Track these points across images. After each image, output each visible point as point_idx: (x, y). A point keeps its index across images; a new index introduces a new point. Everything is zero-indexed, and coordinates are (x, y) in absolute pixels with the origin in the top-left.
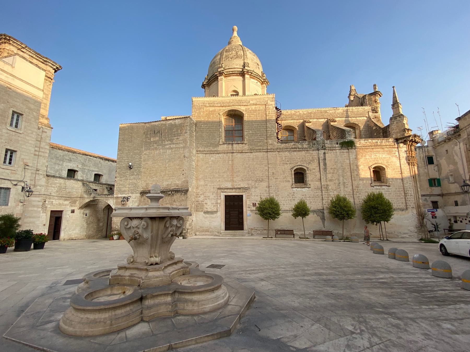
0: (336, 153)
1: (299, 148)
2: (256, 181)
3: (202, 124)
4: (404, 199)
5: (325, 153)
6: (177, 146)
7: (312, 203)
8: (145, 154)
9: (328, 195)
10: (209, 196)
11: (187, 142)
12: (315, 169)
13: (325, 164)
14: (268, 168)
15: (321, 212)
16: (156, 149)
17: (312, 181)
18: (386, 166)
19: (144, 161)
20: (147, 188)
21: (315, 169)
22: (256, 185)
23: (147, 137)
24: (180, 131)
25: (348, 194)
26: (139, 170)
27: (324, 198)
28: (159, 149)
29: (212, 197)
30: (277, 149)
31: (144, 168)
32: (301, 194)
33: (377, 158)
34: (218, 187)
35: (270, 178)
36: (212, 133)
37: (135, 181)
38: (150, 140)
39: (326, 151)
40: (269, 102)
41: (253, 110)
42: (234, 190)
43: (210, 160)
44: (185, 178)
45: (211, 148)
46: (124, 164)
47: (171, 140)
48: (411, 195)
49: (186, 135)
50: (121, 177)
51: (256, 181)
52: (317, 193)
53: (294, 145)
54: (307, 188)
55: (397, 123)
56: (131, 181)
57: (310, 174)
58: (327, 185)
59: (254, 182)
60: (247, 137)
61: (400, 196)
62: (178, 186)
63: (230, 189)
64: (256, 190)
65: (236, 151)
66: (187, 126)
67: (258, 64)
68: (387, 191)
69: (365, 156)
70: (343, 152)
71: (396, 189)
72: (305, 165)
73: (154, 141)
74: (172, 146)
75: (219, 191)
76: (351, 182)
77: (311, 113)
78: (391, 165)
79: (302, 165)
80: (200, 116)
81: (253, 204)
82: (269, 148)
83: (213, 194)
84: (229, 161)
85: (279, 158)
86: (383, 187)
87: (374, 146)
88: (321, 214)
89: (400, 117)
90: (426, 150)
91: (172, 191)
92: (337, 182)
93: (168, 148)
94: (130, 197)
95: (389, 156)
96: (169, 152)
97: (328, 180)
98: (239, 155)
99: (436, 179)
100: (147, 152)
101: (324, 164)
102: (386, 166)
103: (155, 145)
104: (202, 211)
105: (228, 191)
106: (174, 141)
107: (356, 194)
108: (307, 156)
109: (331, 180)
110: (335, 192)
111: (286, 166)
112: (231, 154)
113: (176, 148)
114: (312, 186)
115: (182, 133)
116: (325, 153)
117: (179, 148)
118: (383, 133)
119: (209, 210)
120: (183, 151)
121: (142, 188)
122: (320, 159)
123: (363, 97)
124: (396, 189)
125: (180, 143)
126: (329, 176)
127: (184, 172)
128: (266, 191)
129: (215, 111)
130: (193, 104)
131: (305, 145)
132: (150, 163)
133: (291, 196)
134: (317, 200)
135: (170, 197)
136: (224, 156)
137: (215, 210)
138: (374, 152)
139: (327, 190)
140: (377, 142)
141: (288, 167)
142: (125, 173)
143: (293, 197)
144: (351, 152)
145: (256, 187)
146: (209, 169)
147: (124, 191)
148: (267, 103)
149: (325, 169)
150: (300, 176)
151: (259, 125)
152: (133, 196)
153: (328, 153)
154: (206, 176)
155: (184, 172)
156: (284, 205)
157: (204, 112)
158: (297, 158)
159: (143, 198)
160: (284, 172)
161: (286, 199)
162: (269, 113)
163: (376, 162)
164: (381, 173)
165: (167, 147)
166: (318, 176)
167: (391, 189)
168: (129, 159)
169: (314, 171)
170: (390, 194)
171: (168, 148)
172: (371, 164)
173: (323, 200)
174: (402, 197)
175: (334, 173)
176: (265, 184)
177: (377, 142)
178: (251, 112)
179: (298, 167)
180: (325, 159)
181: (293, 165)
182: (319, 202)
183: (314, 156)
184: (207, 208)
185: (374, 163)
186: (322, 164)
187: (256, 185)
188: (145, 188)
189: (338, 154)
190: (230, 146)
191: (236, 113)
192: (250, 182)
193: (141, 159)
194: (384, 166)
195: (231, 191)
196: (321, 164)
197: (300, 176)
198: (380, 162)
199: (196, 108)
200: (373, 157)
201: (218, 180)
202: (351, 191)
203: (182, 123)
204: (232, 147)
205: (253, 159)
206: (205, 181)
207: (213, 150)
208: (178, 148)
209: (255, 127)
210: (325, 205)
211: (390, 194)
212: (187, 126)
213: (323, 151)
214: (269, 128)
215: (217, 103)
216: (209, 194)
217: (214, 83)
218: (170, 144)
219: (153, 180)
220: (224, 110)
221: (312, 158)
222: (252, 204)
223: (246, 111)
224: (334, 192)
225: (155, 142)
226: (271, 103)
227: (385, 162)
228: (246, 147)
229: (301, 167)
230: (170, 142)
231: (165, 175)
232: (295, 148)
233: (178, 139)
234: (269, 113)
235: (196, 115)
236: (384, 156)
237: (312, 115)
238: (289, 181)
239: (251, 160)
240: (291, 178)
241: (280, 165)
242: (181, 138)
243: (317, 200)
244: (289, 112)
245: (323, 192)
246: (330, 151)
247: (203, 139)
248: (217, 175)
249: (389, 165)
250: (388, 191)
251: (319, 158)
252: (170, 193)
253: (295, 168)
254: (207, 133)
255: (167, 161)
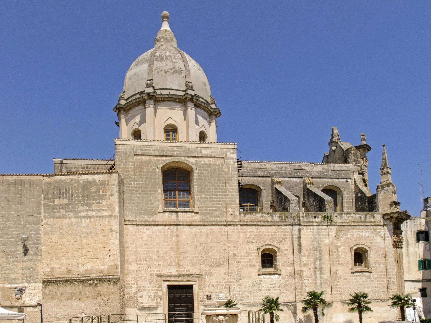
0: (313, 229)
1: (268, 221)
2: (211, 265)
3: (131, 181)
4: (385, 288)
5: (299, 230)
6: (99, 214)
7: (283, 294)
8: (46, 224)
9: (302, 283)
10: (144, 287)
11: (115, 210)
12: (287, 250)
13: (300, 245)
14: (228, 247)
15: (292, 305)
16: (64, 217)
17: (283, 265)
18: (369, 247)
19: (45, 233)
20: (54, 275)
21: (287, 250)
22: (211, 271)
23: (48, 198)
24: (103, 192)
25: (326, 283)
26: (37, 248)
27: (297, 287)
28: (70, 218)
29: (148, 287)
30: (240, 221)
31: (45, 245)
32: (272, 285)
33: (360, 238)
34: (157, 273)
35: (230, 262)
36: (146, 194)
37: (32, 264)
38: (54, 202)
39: (302, 227)
40: (228, 154)
41: (206, 164)
42: (180, 279)
43: (144, 235)
44: (113, 261)
45: (146, 218)
46: (11, 238)
47: (89, 205)
48: (393, 283)
49: (111, 198)
50: (8, 258)
51: (211, 265)
52: (288, 280)
53: (262, 216)
54: (277, 276)
55: (384, 193)
56: (24, 264)
57: (281, 256)
58: (301, 271)
59: (208, 266)
60: (198, 203)
61: (382, 284)
62: (102, 272)
63: (175, 276)
64: (212, 277)
65: (183, 222)
66: (113, 185)
67: (205, 85)
68: (368, 278)
69: (346, 235)
70: (321, 229)
71: (378, 275)
72: (275, 244)
73: (60, 205)
74: (90, 214)
75: (160, 279)
76: (329, 266)
77: (282, 168)
78: (375, 246)
79: (271, 245)
80: (128, 168)
81: (207, 296)
82: (229, 220)
83: (150, 283)
84: (173, 236)
85: (242, 235)
86: (365, 273)
87: (357, 222)
88: (292, 308)
89: (388, 186)
90: (418, 223)
91: (94, 280)
92: (312, 266)
93: (84, 217)
94: (26, 287)
95: (373, 235)
96: (86, 222)
97: (302, 265)
98: (187, 228)
99: (427, 259)
100: (50, 221)
101: (298, 244)
102: (369, 247)
103: (63, 212)
104: (135, 307)
105: (173, 279)
106: (93, 207)
107: (334, 282)
108: (278, 232)
109: (305, 265)
110: (310, 279)
111: (251, 245)
112: (175, 227)
113: (97, 217)
114: (283, 273)
115: (106, 195)
116: (299, 230)
117: (103, 217)
118: (369, 204)
119: (146, 305)
120: (109, 221)
121: (45, 274)
122: (294, 237)
123: (347, 150)
124: (378, 275)
125: (103, 210)
126: (304, 259)
127: (111, 253)
128: (224, 279)
129: (149, 161)
130: (116, 149)
131: (276, 218)
132: (55, 237)
133: (257, 285)
134: (289, 290)
135: (91, 288)
136: (164, 229)
137: (154, 305)
138: (357, 229)
139: (301, 277)
140: (360, 217)
141: (253, 247)
142: (15, 251)
143: (259, 287)
144: (331, 229)
145: (211, 274)
146: (144, 247)
147: (15, 279)
148: (226, 155)
149: (300, 251)
150: (268, 259)
151: (214, 186)
152: (31, 286)
153: (303, 229)
154: (140, 258)
155: (111, 253)
156: (248, 296)
157: (133, 162)
158: (265, 235)
159: (47, 289)
160: (248, 253)
161: (251, 289)
162: (229, 170)
163: (358, 242)
164: (363, 256)
165: (83, 214)
166: (291, 260)
167: (373, 275)
168: (19, 231)
169: (286, 252)
170: (371, 281)
171: (84, 217)
172: (352, 245)
173: (295, 289)
174: (384, 285)
175: (310, 256)
176: (223, 270)
177: (360, 217)
178: (203, 167)
179: (267, 247)
180: (299, 238)
181: (260, 245)
182: (291, 293)
183: (287, 232)
184: (142, 303)
185: (356, 243)
186: (296, 244)
187: (211, 271)
188: (50, 274)
189: (315, 230)
190: (174, 215)
191: (181, 166)
192: (203, 267)
193: (39, 230)
194: (367, 248)
195: (176, 279)
196: (294, 243)
197: (268, 259)
198: (362, 242)
199: (121, 156)
200: (355, 236)
201: (157, 264)
202: (329, 279)
203: (105, 181)
204: (177, 216)
205: (207, 235)
206: (138, 264)
207: (149, 219)
208: (100, 217)
209: (209, 189)
210: (297, 295)
211: (371, 281)
212: (113, 185)
213: (298, 227)
214: (229, 191)
215: (154, 150)
216: (144, 284)
217: (137, 108)
218: (87, 211)
219: (62, 264)
220: (164, 161)
221: (285, 235)
222: (206, 297)
223: (196, 164)
224: (308, 280)
225: (61, 206)
226: (232, 156)
227: (369, 242)
228: (197, 218)
229: (270, 247)
230: (87, 208)
231: (81, 256)
232: (263, 221)
233: (99, 203)
234: (229, 170)
235: (122, 166)
236: (367, 235)
237: (283, 171)
238: (254, 266)
239: (204, 237)
240: (258, 261)
241: (243, 244)
242: (104, 203)
243: (289, 290)
244: (252, 165)
245: (296, 279)
246: (306, 227)
247: (133, 203)
248: (155, 257)
249: (372, 246)
250: (369, 278)
251: (293, 236)
252: (92, 282)
253: (263, 248)
254: (139, 194)
255: (83, 235)
